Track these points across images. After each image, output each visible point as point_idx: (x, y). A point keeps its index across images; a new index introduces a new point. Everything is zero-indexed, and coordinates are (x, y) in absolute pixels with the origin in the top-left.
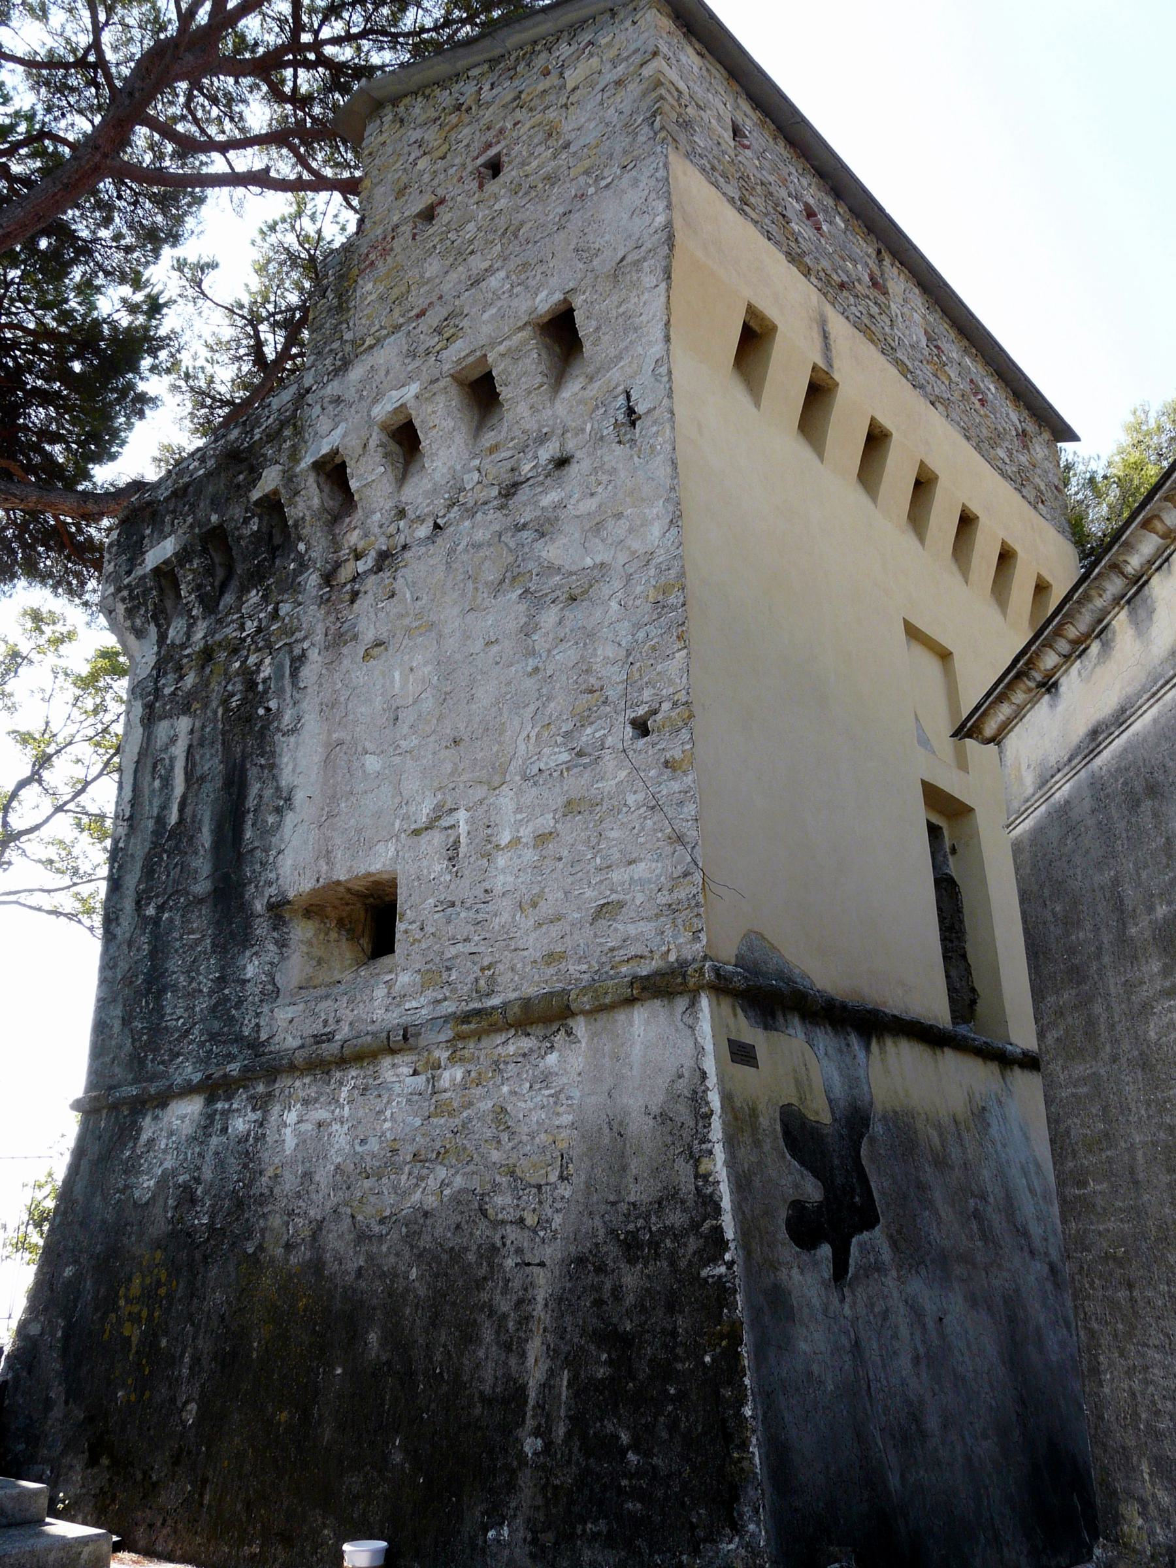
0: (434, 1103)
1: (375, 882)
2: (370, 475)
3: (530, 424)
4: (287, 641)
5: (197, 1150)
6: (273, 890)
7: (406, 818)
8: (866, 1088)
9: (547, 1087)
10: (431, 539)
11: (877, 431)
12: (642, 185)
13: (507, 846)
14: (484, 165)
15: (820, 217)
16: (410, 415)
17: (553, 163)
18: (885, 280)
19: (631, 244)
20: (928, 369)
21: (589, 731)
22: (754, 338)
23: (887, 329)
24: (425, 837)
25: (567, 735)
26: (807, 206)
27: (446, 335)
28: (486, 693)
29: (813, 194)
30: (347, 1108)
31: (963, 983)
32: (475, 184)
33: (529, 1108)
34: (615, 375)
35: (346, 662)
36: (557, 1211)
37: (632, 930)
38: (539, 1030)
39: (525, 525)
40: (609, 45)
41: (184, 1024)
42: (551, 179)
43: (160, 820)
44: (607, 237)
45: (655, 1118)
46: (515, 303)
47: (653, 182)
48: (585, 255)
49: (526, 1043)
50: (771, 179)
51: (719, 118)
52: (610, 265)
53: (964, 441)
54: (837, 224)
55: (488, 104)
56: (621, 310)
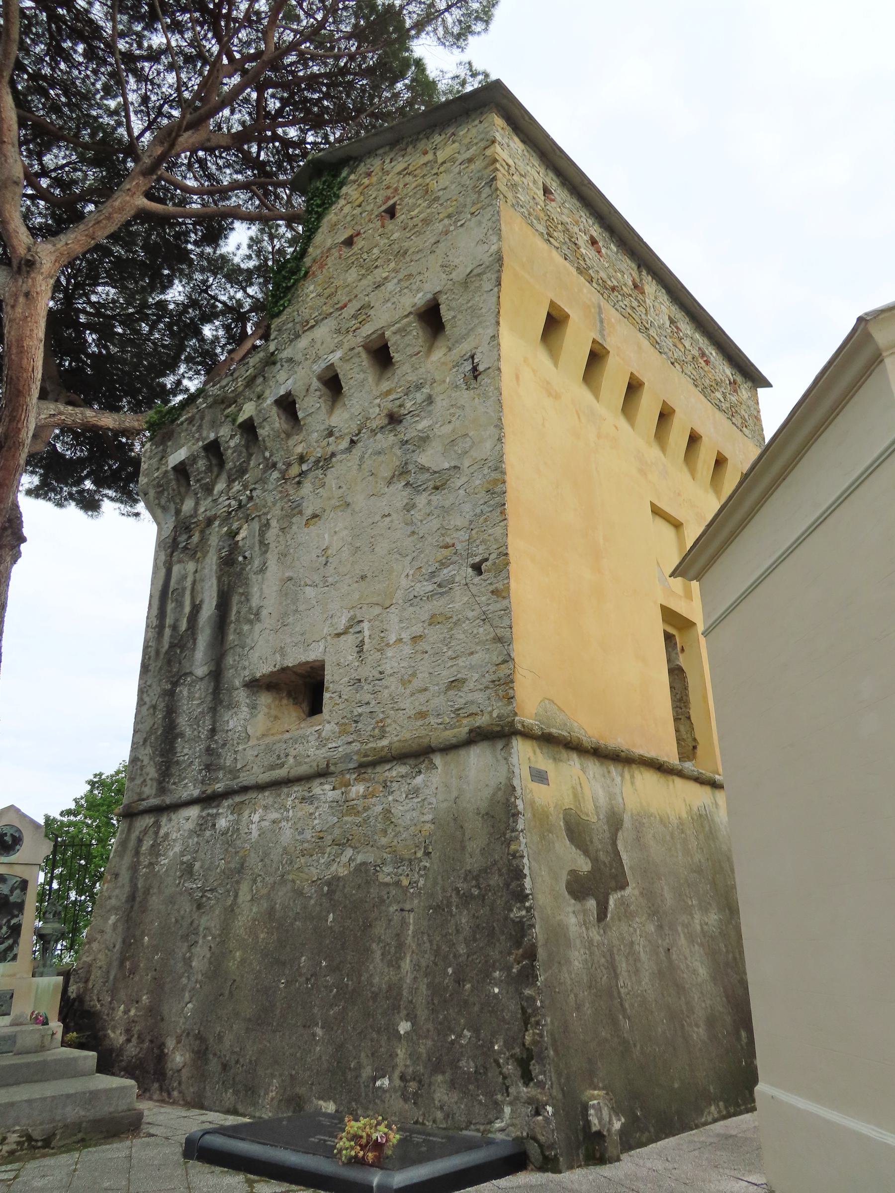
0: (345, 807)
1: (311, 667)
2: (311, 406)
3: (412, 377)
4: (258, 514)
5: (196, 839)
6: (247, 673)
7: (332, 625)
8: (621, 800)
9: (417, 797)
10: (349, 450)
11: (634, 383)
12: (483, 225)
13: (394, 644)
14: (385, 211)
15: (601, 244)
16: (336, 371)
17: (429, 211)
18: (643, 284)
19: (476, 263)
20: (669, 342)
21: (445, 571)
22: (554, 323)
23: (643, 316)
24: (343, 638)
25: (433, 574)
26: (592, 238)
27: (360, 320)
28: (382, 547)
29: (595, 231)
30: (291, 812)
31: (689, 735)
32: (379, 223)
33: (405, 811)
34: (465, 347)
35: (294, 527)
36: (422, 876)
37: (470, 697)
38: (412, 762)
39: (407, 441)
40: (465, 136)
41: (188, 759)
42: (426, 222)
43: (175, 628)
44: (461, 258)
45: (483, 816)
46: (403, 300)
47: (490, 224)
48: (447, 269)
49: (403, 769)
50: (568, 220)
51: (535, 182)
52: (462, 276)
53: (694, 387)
54: (611, 249)
55: (388, 173)
56: (469, 305)
